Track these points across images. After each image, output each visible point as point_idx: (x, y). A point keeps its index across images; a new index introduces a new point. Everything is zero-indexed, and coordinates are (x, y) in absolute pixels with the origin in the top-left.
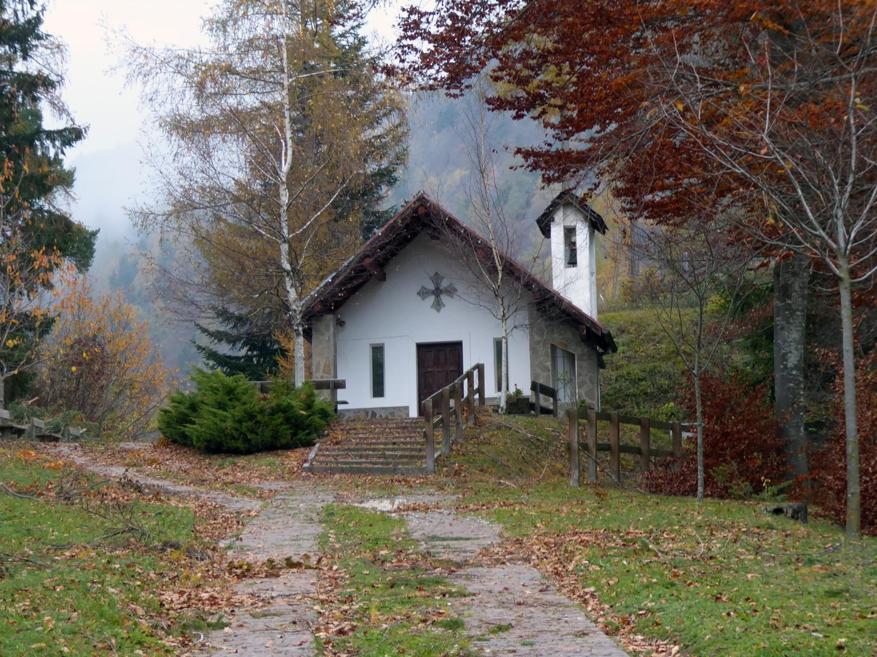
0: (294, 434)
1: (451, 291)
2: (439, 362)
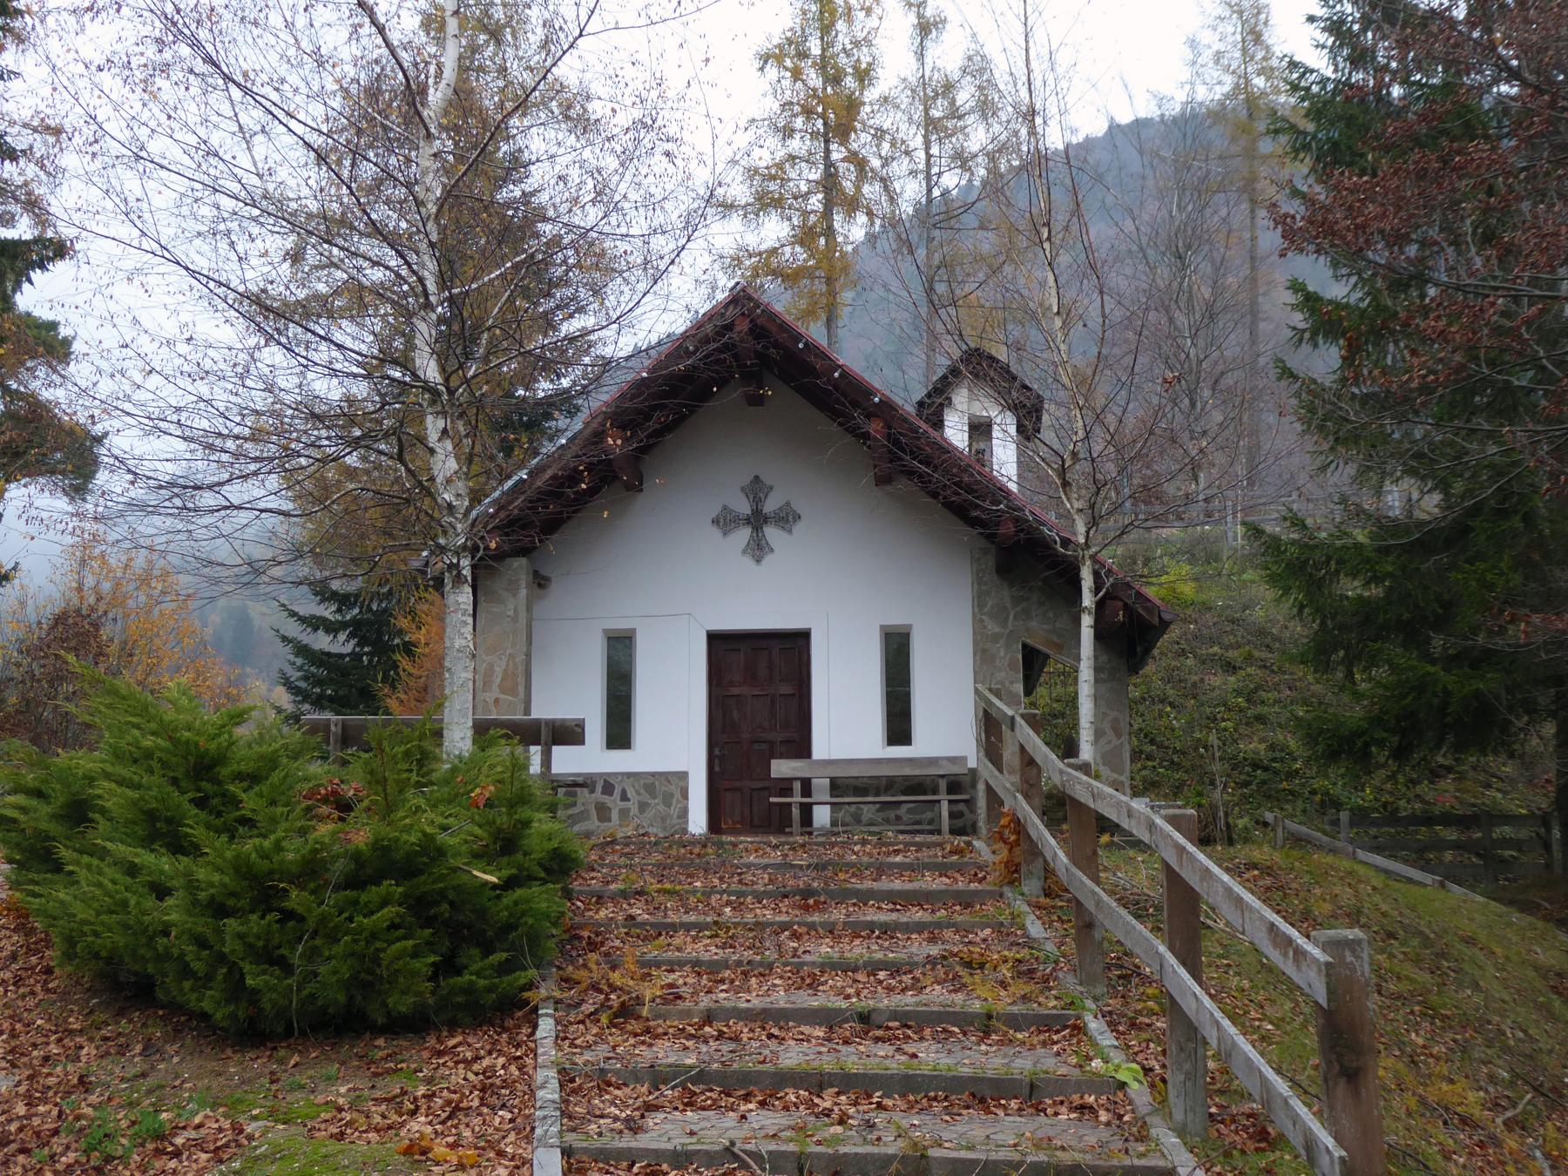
0: (449, 966)
1: (787, 519)
2: (759, 681)
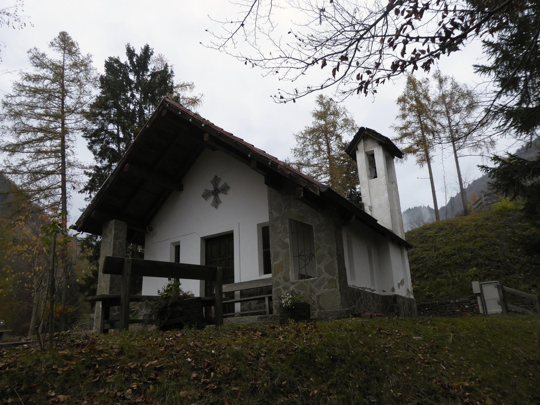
1: (225, 190)
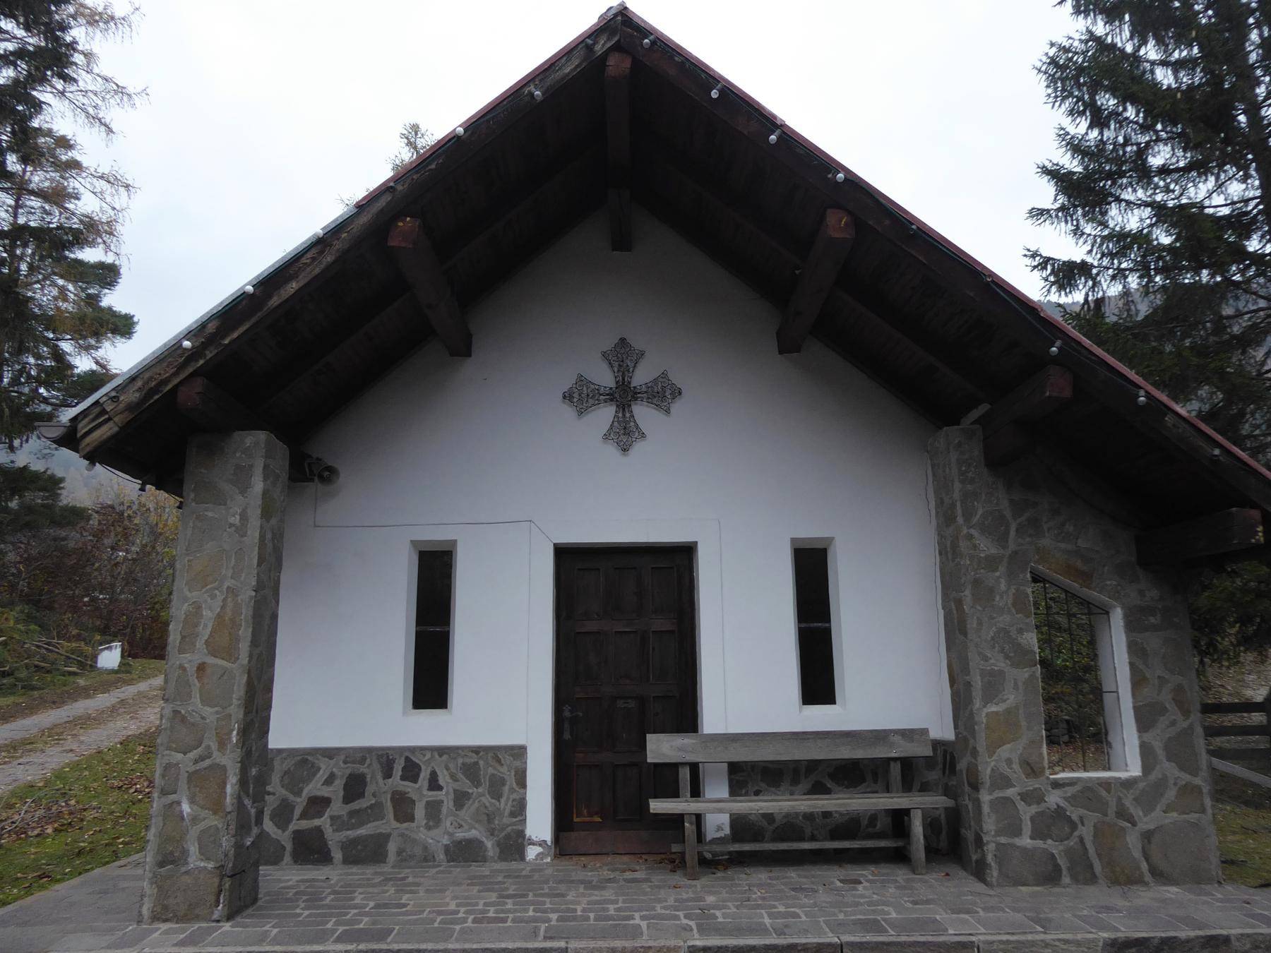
1: (663, 394)
2: (624, 619)
